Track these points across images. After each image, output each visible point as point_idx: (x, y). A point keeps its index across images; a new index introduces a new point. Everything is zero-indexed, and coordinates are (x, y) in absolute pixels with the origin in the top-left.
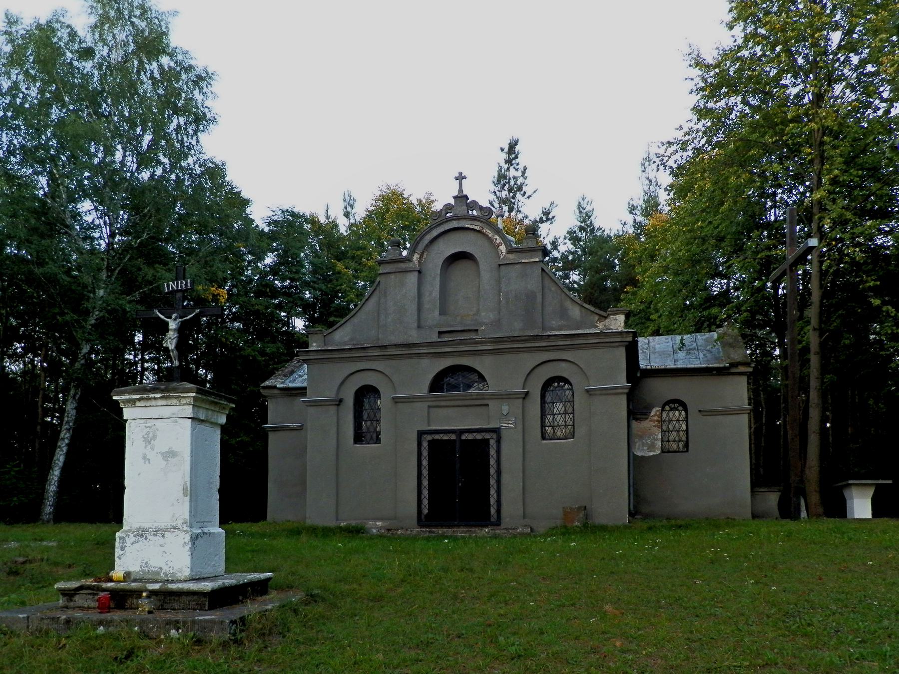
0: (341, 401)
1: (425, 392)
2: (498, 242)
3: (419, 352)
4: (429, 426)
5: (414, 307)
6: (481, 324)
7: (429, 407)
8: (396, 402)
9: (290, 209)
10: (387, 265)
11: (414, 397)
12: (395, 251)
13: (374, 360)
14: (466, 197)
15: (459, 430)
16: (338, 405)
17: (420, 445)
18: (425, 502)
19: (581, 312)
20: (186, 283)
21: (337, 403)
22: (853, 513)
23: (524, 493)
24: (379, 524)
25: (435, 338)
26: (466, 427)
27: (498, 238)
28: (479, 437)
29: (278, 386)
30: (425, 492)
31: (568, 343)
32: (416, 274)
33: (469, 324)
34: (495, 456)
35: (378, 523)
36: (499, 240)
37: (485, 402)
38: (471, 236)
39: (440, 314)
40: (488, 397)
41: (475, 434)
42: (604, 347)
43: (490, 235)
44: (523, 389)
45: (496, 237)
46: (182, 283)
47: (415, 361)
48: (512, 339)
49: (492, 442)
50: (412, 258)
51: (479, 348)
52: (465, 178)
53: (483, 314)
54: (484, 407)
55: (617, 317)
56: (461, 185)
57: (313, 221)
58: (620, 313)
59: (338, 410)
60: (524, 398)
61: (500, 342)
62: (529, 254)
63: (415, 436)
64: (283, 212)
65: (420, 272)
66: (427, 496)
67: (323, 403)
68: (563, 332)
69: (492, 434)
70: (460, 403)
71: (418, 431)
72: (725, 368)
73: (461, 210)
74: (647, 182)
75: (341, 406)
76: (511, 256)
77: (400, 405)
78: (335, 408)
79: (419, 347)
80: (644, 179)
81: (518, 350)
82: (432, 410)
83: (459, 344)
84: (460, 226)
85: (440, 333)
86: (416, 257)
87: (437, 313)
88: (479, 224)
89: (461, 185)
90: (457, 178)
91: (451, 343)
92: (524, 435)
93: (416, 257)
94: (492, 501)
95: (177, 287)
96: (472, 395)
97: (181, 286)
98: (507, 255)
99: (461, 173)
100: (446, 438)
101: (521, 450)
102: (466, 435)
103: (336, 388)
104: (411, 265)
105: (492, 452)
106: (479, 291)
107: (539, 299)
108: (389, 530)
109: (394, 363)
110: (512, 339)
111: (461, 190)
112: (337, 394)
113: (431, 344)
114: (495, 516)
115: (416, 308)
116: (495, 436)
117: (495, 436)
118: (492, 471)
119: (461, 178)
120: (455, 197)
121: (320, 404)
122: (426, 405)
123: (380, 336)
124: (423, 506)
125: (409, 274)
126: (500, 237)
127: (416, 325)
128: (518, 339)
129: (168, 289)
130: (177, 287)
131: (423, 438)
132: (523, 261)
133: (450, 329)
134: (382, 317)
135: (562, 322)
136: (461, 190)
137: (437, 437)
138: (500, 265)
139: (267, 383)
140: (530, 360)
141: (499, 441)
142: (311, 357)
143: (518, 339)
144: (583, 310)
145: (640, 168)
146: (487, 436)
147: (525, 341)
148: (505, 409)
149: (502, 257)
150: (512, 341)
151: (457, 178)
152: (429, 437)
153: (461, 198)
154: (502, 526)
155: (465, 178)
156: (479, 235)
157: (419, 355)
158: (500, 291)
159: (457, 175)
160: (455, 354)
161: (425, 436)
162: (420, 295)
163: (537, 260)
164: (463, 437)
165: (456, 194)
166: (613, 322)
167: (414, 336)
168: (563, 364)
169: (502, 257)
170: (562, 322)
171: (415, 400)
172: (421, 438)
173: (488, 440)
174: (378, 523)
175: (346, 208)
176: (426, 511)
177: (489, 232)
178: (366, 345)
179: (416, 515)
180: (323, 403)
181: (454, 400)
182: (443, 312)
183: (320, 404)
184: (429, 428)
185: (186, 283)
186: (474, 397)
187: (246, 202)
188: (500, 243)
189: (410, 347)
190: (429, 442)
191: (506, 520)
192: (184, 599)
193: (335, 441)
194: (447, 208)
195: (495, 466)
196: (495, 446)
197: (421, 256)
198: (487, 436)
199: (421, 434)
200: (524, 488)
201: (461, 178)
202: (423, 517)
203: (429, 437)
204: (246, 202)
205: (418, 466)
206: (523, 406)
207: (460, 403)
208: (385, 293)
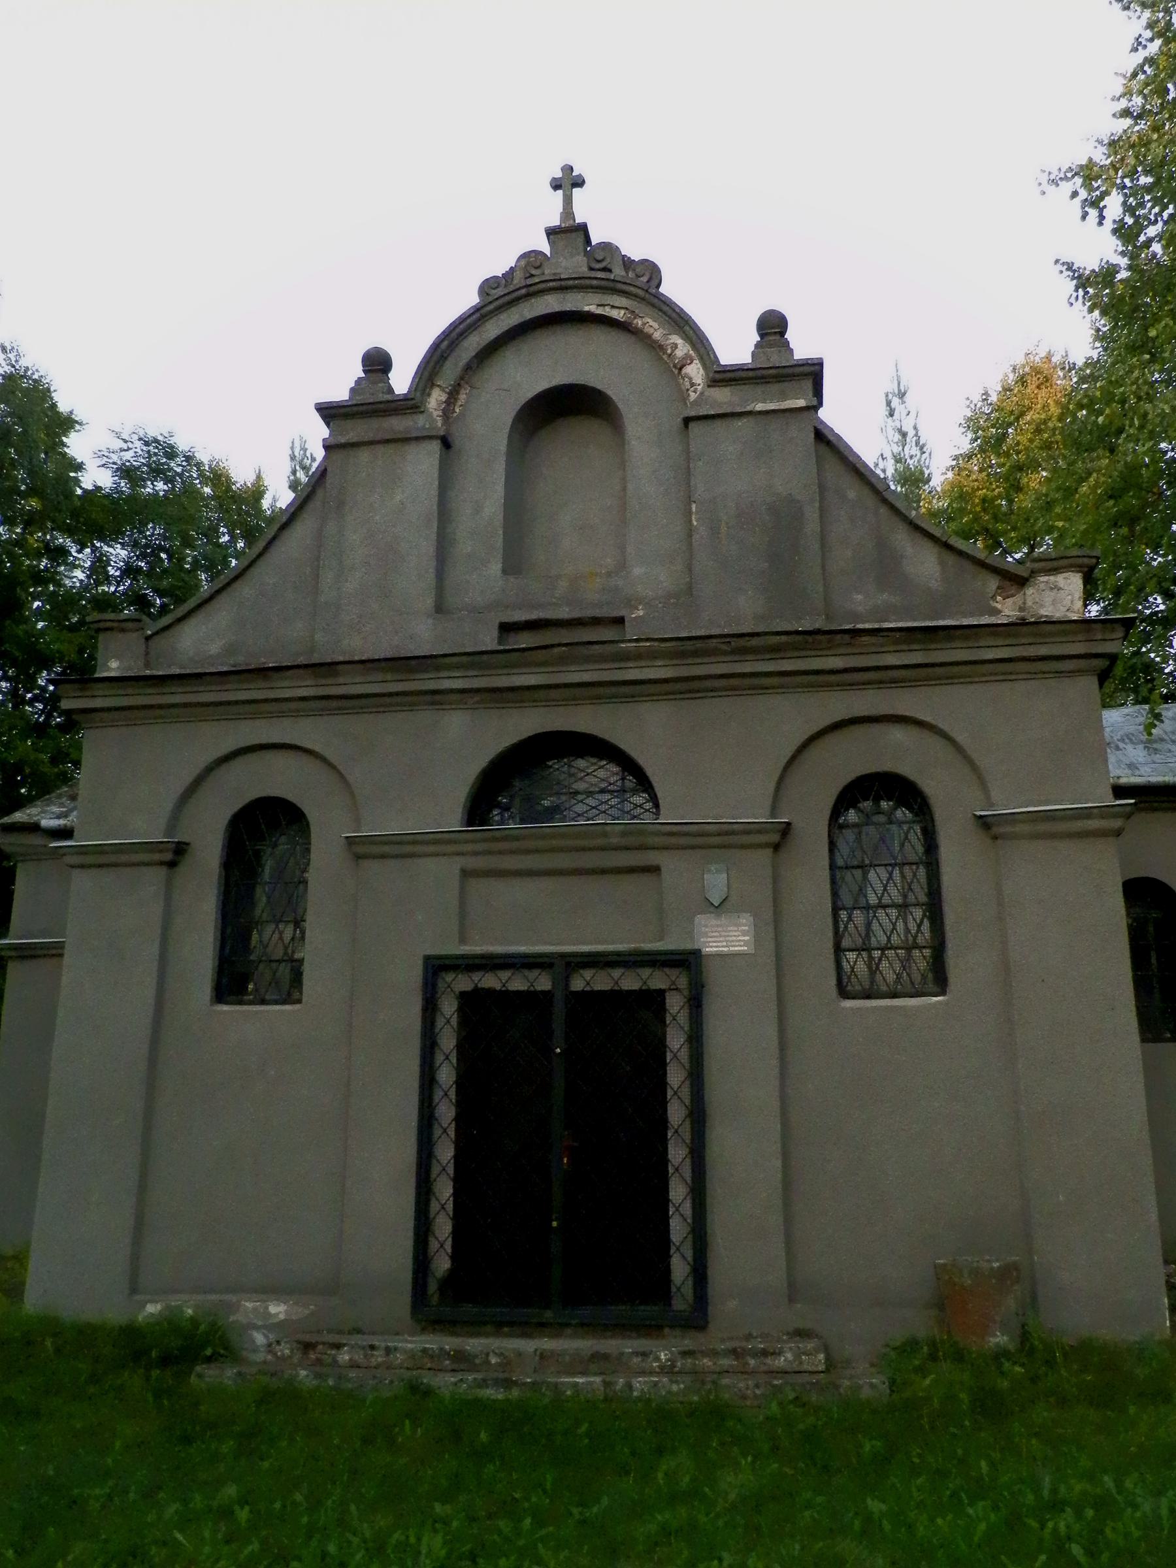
0: (181, 849)
1: (453, 821)
2: (679, 353)
3: (432, 685)
4: (463, 940)
5: (426, 546)
6: (631, 603)
7: (466, 874)
8: (358, 857)
9: (160, 438)
12: (375, 383)
13: (296, 714)
14: (583, 229)
15: (563, 956)
16: (172, 864)
17: (430, 1007)
18: (443, 1227)
19: (942, 563)
21: (168, 856)
23: (787, 1203)
24: (278, 1310)
25: (489, 640)
26: (585, 948)
27: (680, 341)
28: (630, 982)
29: (45, 823)
30: (444, 1190)
32: (435, 446)
33: (593, 602)
34: (684, 1055)
36: (682, 348)
37: (652, 858)
38: (600, 338)
39: (505, 572)
40: (658, 841)
41: (616, 973)
42: (1032, 676)
43: (657, 335)
44: (773, 815)
45: (676, 339)
47: (424, 717)
48: (735, 643)
49: (675, 1004)
50: (423, 402)
52: (579, 183)
53: (637, 571)
54: (645, 878)
55: (1060, 579)
56: (568, 201)
57: (218, 477)
59: (169, 884)
60: (776, 847)
61: (695, 653)
62: (775, 388)
63: (416, 974)
64: (147, 444)
65: (446, 443)
66: (450, 1207)
67: (124, 858)
69: (673, 973)
73: (574, 265)
74: (897, 437)
75: (182, 869)
76: (724, 398)
77: (374, 866)
78: (163, 871)
79: (438, 668)
80: (891, 432)
81: (754, 684)
82: (479, 887)
83: (563, 660)
85: (506, 628)
86: (436, 399)
87: (496, 567)
89: (568, 201)
90: (556, 185)
91: (541, 655)
92: (779, 976)
93: (436, 399)
94: (678, 1229)
96: (605, 835)
100: (518, 983)
101: (772, 1032)
102: (588, 974)
103: (169, 805)
104: (421, 420)
105: (676, 1040)
106: (623, 507)
107: (812, 525)
108: (308, 1347)
110: (735, 643)
112: (171, 827)
113: (476, 660)
114: (688, 1290)
115: (432, 550)
117: (683, 982)
118: (676, 1113)
120: (551, 233)
121: (113, 858)
122: (458, 863)
123: (318, 637)
124: (434, 1245)
126: (687, 338)
127: (430, 602)
128: (755, 642)
131: (441, 985)
132: (760, 407)
133: (534, 615)
134: (328, 577)
135: (884, 597)
137: (490, 981)
138: (687, 421)
139: (18, 816)
141: (696, 1003)
142: (98, 703)
143: (755, 642)
144: (951, 559)
145: (884, 411)
146: (657, 980)
147: (776, 651)
148: (716, 882)
149: (693, 396)
151: (556, 185)
152: (464, 983)
154: (718, 1335)
155: (579, 183)
157: (436, 698)
158: (689, 500)
159: (559, 174)
160: (554, 694)
161: (449, 977)
162: (444, 513)
163: (801, 403)
164: (578, 984)
165: (555, 221)
166: (1048, 597)
168: (898, 734)
169: (693, 396)
170: (884, 597)
171: (418, 849)
172: (434, 986)
173: (662, 993)
175: (294, 472)
176: (442, 1264)
177: (653, 327)
180: (124, 858)
182: (514, 565)
184: (466, 949)
186: (614, 841)
187: (67, 423)
188: (687, 356)
189: (412, 671)
190: (463, 995)
192: (941, 634)
193: (150, 993)
194: (528, 264)
195: (685, 1093)
196: (683, 1019)
197: (453, 395)
198: (657, 980)
200: (787, 1184)
202: (433, 1287)
203: (464, 983)
204: (67, 423)
205: (422, 1087)
206: (776, 879)
208: (341, 504)
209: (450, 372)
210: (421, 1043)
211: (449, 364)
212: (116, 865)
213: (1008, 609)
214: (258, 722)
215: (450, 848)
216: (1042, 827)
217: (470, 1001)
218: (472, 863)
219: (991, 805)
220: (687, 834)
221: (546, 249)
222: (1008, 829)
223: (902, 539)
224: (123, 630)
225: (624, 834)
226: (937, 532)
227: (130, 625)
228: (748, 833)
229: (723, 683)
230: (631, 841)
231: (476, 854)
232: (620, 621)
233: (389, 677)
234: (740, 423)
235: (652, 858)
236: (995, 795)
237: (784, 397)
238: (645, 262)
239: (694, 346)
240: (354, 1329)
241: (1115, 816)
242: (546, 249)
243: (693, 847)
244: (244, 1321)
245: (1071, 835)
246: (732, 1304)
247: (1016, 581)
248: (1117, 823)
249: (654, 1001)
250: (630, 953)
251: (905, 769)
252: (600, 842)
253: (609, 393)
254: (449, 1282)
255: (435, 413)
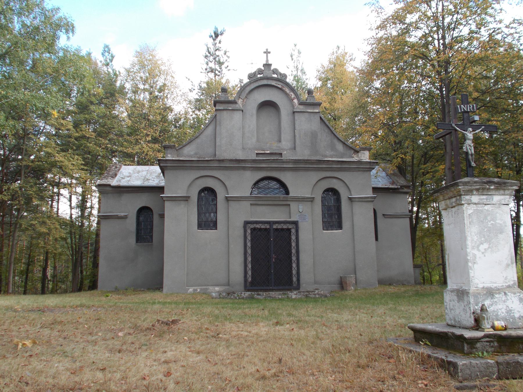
3: (244, 165)
4: (290, 218)
10: (221, 105)
11: (241, 197)
13: (216, 169)
17: (245, 231)
18: (250, 273)
19: (343, 147)
20: (473, 106)
22: (476, 281)
24: (217, 289)
25: (254, 157)
27: (293, 94)
28: (285, 227)
31: (339, 166)
35: (216, 289)
36: (293, 96)
37: (288, 203)
45: (292, 93)
46: (470, 106)
47: (242, 172)
49: (293, 231)
51: (285, 166)
52: (269, 53)
58: (366, 150)
62: (312, 107)
68: (334, 159)
70: (270, 203)
71: (298, 221)
72: (397, 189)
84: (269, 83)
88: (281, 84)
90: (265, 53)
95: (467, 109)
96: (280, 198)
97: (470, 109)
98: (299, 106)
99: (267, 50)
102: (277, 225)
104: (237, 105)
109: (227, 173)
111: (267, 61)
113: (254, 161)
116: (294, 226)
119: (267, 52)
121: (174, 199)
122: (252, 202)
125: (236, 112)
126: (294, 93)
129: (461, 110)
130: (467, 109)
132: (309, 111)
135: (332, 153)
136: (267, 61)
137: (258, 226)
140: (315, 176)
141: (297, 231)
150: (306, 163)
151: (265, 53)
152: (252, 226)
153: (267, 65)
156: (280, 91)
157: (244, 168)
159: (265, 51)
161: (249, 225)
164: (275, 227)
165: (265, 63)
167: (241, 156)
168: (335, 180)
170: (332, 153)
171: (242, 199)
173: (291, 229)
174: (216, 289)
178: (207, 159)
179: (243, 282)
180: (177, 199)
181: (262, 200)
183: (174, 199)
185: (473, 106)
186: (281, 199)
188: (294, 97)
190: (251, 229)
191: (304, 286)
199: (246, 223)
201: (267, 52)
202: (248, 284)
207: (270, 203)
209: (244, 95)
210: (98, 260)
211: (243, 93)
212: (176, 200)
213: (355, 158)
214: (205, 171)
215: (248, 199)
216: (361, 200)
217: (253, 230)
218: (252, 202)
219: (351, 195)
220: (295, 198)
221: (263, 68)
222: (354, 200)
223: (336, 141)
224: (171, 148)
225: (283, 198)
226: (343, 141)
227: (173, 147)
228: (306, 199)
229: (303, 168)
230: (285, 199)
231: (253, 201)
232: (281, 154)
233: (235, 163)
234: (305, 114)
235: (288, 203)
236: (352, 193)
237: (314, 109)
238: (284, 74)
239: (296, 96)
240: (148, 328)
241: (373, 198)
242: (263, 68)
243: (296, 201)
244: (210, 291)
245: (364, 201)
246: (304, 285)
247: (356, 152)
248: (373, 200)
249: (289, 230)
250: (285, 221)
251: (336, 187)
252: (279, 199)
253: (277, 103)
254: (252, 283)
255: (240, 104)
